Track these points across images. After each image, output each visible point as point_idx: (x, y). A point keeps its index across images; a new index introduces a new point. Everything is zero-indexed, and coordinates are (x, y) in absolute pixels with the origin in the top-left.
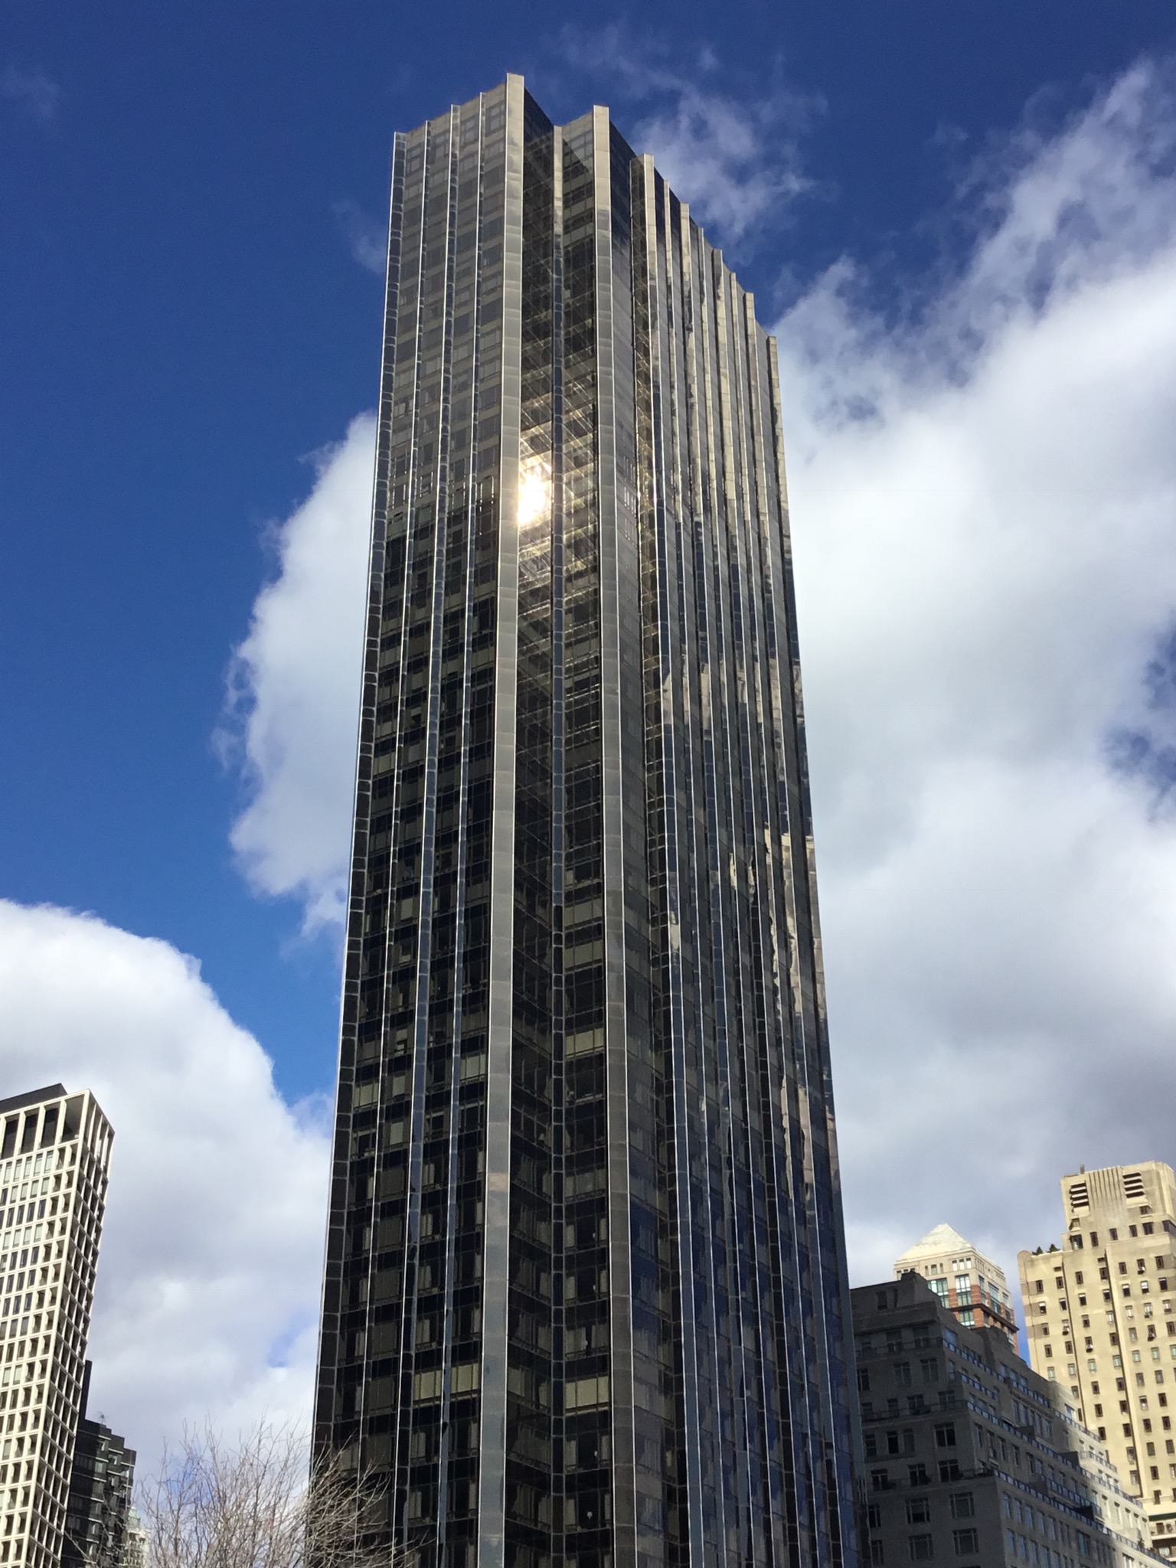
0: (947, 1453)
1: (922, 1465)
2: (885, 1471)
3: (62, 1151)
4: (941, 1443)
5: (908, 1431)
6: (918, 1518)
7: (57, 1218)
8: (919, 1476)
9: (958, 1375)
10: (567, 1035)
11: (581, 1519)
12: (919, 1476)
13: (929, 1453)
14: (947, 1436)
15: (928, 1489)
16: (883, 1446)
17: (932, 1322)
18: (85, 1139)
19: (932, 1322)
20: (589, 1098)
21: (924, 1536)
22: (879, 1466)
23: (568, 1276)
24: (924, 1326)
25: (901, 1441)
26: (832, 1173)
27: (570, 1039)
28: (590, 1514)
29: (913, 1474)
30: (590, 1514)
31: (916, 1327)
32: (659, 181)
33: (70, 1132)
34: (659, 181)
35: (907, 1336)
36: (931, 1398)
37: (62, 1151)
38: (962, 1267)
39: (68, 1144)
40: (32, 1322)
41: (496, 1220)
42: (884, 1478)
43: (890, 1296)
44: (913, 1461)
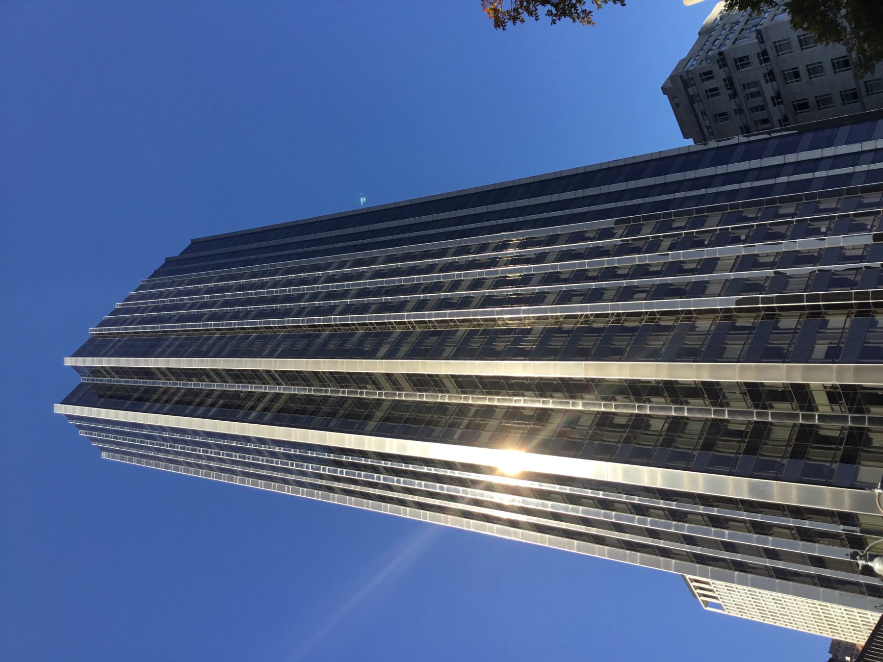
0: (755, 60)
1: (765, 75)
2: (772, 98)
4: (718, 94)
5: (744, 87)
6: (797, 75)
10: (817, 410)
12: (770, 76)
13: (756, 71)
14: (742, 62)
15: (776, 71)
17: (681, 77)
19: (681, 77)
21: (808, 70)
24: (684, 82)
25: (753, 90)
27: (820, 408)
32: (104, 324)
34: (104, 324)
35: (691, 91)
41: (735, 487)
43: (676, 101)
44: (763, 82)
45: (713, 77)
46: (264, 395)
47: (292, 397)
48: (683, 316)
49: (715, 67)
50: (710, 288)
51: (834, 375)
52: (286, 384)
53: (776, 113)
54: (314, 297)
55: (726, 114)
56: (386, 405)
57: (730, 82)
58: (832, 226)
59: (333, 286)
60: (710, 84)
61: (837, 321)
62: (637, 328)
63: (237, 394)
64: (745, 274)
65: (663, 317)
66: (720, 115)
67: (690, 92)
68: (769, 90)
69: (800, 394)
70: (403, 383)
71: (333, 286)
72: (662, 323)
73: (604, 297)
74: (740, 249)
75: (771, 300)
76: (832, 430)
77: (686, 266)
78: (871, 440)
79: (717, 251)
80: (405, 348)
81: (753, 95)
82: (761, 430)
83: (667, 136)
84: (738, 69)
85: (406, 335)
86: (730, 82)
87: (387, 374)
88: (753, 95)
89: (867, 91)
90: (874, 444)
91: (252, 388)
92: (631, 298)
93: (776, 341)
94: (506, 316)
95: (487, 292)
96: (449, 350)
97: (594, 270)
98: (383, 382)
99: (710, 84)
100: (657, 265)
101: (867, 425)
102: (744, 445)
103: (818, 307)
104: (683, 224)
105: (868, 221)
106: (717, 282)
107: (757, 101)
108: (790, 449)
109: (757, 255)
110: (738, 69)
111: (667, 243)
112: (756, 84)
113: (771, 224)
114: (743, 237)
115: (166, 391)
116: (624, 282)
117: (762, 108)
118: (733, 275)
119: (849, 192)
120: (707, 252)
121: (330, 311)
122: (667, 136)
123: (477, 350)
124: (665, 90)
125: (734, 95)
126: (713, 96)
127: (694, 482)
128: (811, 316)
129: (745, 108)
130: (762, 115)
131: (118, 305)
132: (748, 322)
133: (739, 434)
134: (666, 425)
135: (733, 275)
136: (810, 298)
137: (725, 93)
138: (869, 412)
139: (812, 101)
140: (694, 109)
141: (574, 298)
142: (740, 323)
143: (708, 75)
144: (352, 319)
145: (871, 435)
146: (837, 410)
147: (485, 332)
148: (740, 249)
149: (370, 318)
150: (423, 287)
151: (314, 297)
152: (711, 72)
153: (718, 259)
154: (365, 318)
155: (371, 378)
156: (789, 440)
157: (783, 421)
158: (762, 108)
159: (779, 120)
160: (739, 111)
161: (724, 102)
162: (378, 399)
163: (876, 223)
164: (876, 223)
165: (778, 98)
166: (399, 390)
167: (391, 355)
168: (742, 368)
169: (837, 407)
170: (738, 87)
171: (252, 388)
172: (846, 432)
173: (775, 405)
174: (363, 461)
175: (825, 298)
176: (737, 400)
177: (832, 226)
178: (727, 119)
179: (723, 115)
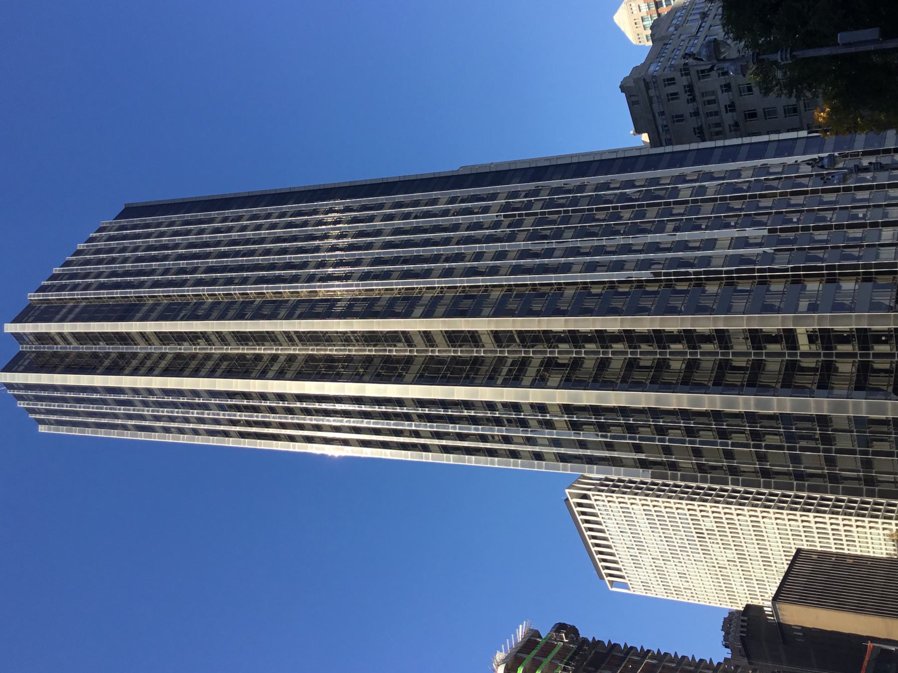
1: (721, 86)
3: (596, 500)
4: (677, 98)
5: (703, 95)
7: (629, 502)
8: (727, 87)
9: (671, 66)
11: (885, 342)
15: (733, 84)
16: (713, 108)
17: (644, 80)
18: (589, 490)
19: (644, 80)
20: (516, 336)
22: (723, 109)
23: (669, 348)
24: (647, 84)
26: (614, 156)
28: (883, 338)
29: (726, 91)
30: (883, 338)
31: (648, 89)
32: (43, 289)
33: (585, 497)
35: (652, 92)
36: (684, 81)
37: (596, 500)
38: (635, 8)
39: (593, 498)
40: (679, 511)
42: (730, 106)
43: (634, 99)
44: (719, 92)
45: (674, 83)
46: (275, 358)
47: (311, 358)
48: (608, 285)
49: (677, 75)
50: (575, 268)
51: (619, 324)
52: (303, 345)
53: (728, 119)
54: (166, 272)
55: (682, 116)
56: (282, 358)
57: (690, 88)
58: (739, 221)
59: (183, 263)
60: (671, 89)
61: (813, 286)
62: (601, 295)
63: (242, 357)
64: (741, 251)
65: (678, 283)
66: (677, 116)
67: (646, 95)
68: (724, 99)
69: (722, 338)
70: (154, 339)
71: (183, 263)
72: (620, 290)
73: (500, 273)
74: (734, 233)
75: (764, 270)
76: (740, 362)
77: (691, 245)
78: (837, 368)
79: (716, 234)
80: (232, 313)
81: (710, 102)
82: (577, 363)
83: (624, 135)
84: (699, 79)
85: (156, 305)
86: (690, 88)
87: (141, 333)
88: (710, 102)
89: (805, 107)
90: (840, 370)
91: (260, 350)
92: (594, 271)
93: (704, 302)
94: (323, 290)
95: (366, 268)
96: (486, 311)
97: (611, 246)
98: (138, 339)
99: (671, 89)
100: (667, 243)
101: (834, 359)
102: (893, 379)
103: (765, 277)
104: (682, 211)
105: (764, 218)
106: (718, 257)
107: (713, 108)
108: (781, 376)
109: (747, 237)
110: (699, 79)
111: (670, 226)
112: (713, 93)
113: (755, 214)
114: (733, 224)
115: (148, 356)
116: (642, 256)
117: (716, 113)
118: (731, 252)
119: (845, 189)
120: (707, 234)
121: (183, 283)
122: (624, 135)
123: (515, 310)
124: (623, 88)
125: (693, 100)
126: (672, 99)
127: (712, 402)
128: (727, 284)
129: (701, 113)
130: (714, 119)
131: (57, 270)
132: (599, 291)
133: (564, 365)
134: (684, 366)
135: (731, 252)
136: (793, 269)
137: (684, 97)
138: (700, 348)
139: (760, 112)
140: (652, 109)
141: (598, 268)
142: (594, 291)
143: (671, 81)
144: (173, 291)
145: (838, 365)
146: (814, 348)
147: (404, 299)
148: (734, 233)
149: (188, 291)
150: (444, 257)
151: (166, 272)
152: (673, 79)
153: (716, 239)
154: (184, 291)
155: (270, 337)
156: (780, 371)
157: (590, 354)
158: (716, 113)
159: (729, 125)
160: (696, 114)
161: (682, 106)
162: (476, 357)
163: (835, 216)
164: (835, 216)
165: (731, 107)
166: (226, 345)
167: (144, 318)
168: (539, 321)
169: (813, 347)
170: (697, 93)
171: (260, 350)
172: (820, 364)
173: (614, 345)
174: (95, 396)
175: (675, 274)
176: (740, 344)
177: (739, 221)
178: (683, 120)
179: (679, 118)
